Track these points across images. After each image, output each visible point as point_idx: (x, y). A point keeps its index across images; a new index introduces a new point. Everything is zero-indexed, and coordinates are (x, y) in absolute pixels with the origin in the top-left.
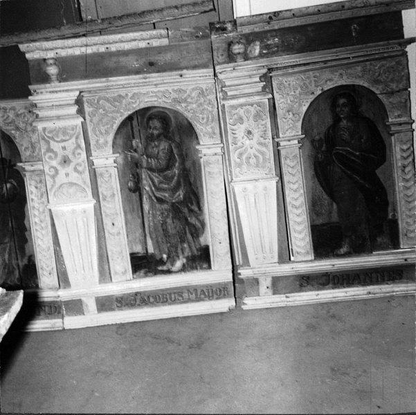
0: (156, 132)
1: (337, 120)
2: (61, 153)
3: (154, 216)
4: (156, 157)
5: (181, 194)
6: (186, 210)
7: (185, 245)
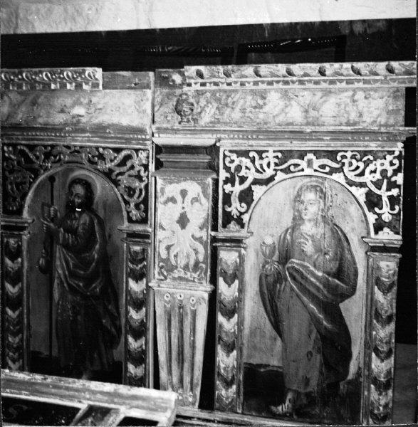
5: (97, 287)
6: (101, 310)
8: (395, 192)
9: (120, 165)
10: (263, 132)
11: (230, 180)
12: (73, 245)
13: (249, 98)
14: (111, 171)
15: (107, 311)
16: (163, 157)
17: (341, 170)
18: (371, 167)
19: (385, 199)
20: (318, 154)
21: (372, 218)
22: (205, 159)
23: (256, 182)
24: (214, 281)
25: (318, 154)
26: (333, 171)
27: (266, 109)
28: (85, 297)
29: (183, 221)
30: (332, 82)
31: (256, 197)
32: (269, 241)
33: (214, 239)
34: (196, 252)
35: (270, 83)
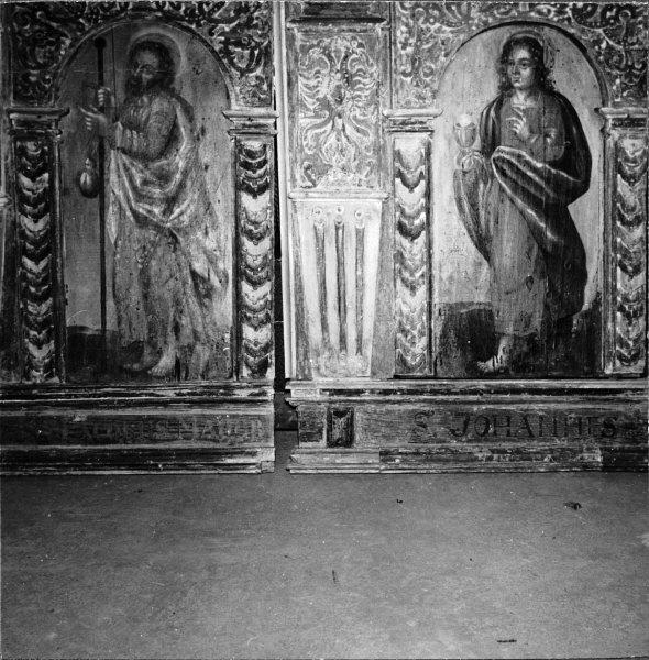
1: (506, 89)
32: (465, 121)
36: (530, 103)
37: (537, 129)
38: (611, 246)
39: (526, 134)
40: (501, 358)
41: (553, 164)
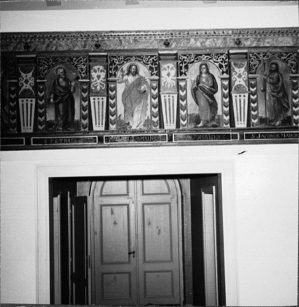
0: (273, 69)
1: (201, 73)
2: (238, 72)
3: (270, 102)
4: (273, 79)
5: (281, 95)
6: (283, 101)
7: (282, 115)
8: (226, 64)
9: (288, 57)
10: (191, 49)
11: (182, 63)
12: (100, 90)
13: (185, 40)
14: (285, 59)
15: (285, 101)
16: (161, 57)
17: (212, 59)
18: (220, 58)
19: (224, 66)
20: (206, 55)
21: (221, 71)
22: (175, 57)
23: (189, 63)
24: (178, 91)
25: (135, 57)
26: (210, 59)
27: (190, 43)
28: (278, 98)
29: (169, 75)
30: (208, 36)
31: (189, 67)
32: (193, 79)
33: (178, 79)
34: (173, 83)
35: (192, 36)
36: (206, 76)
37: (207, 80)
38: (223, 102)
39: (205, 81)
40: (201, 125)
41: (211, 87)
